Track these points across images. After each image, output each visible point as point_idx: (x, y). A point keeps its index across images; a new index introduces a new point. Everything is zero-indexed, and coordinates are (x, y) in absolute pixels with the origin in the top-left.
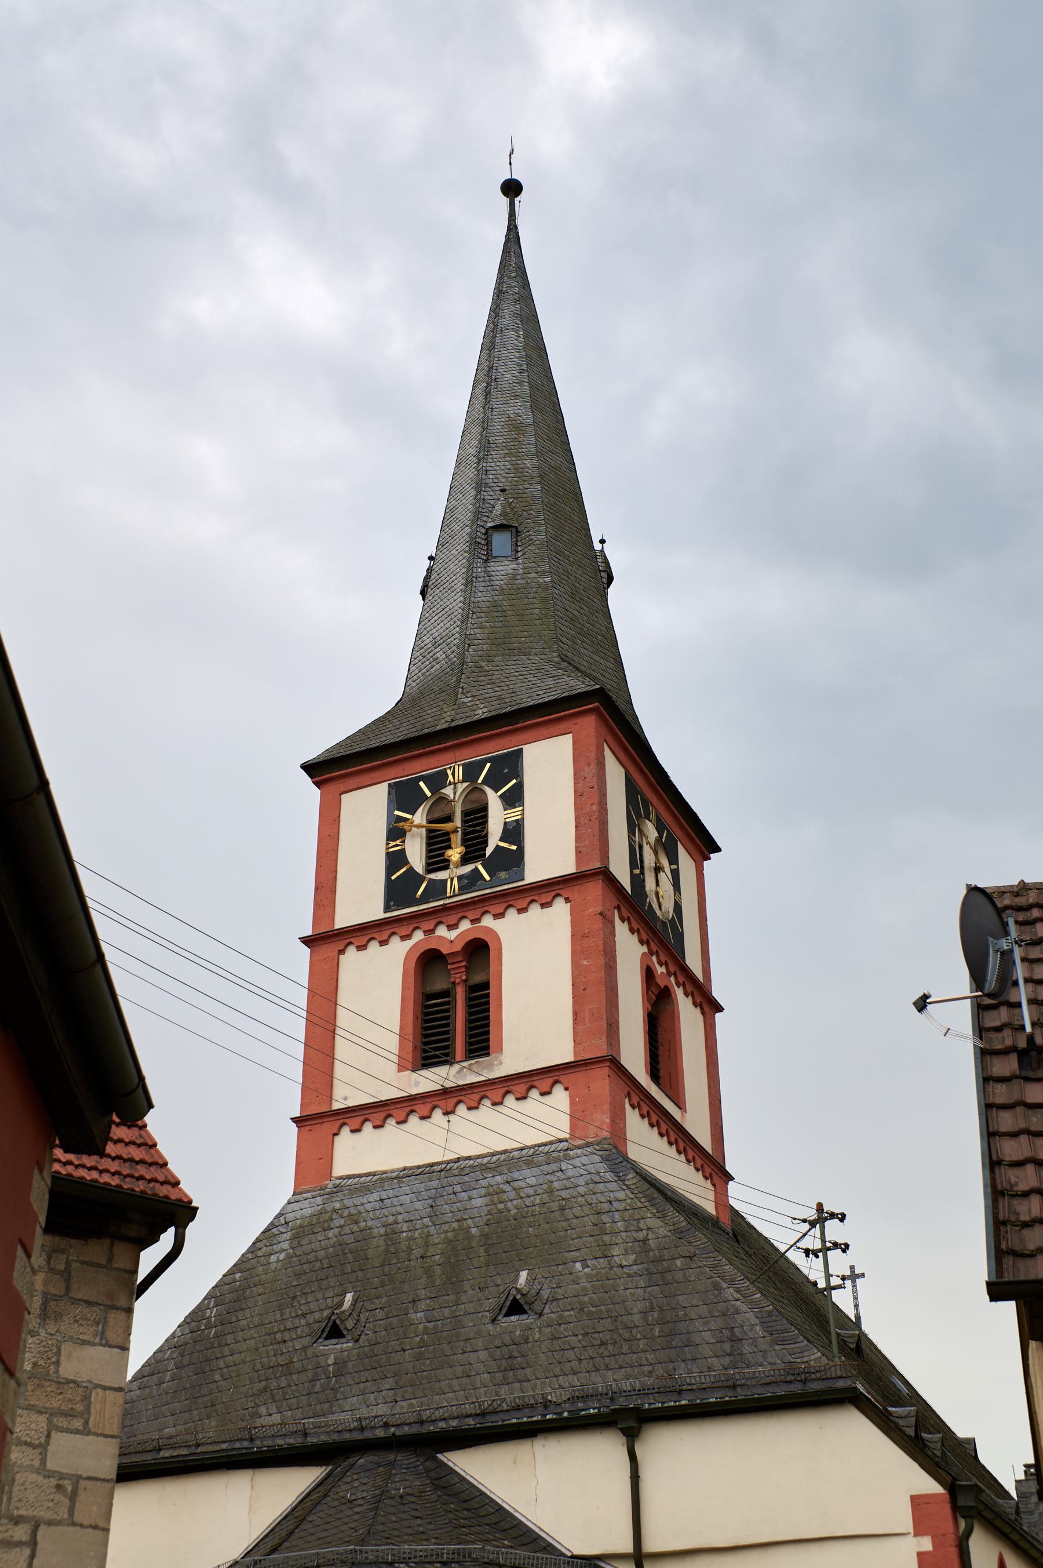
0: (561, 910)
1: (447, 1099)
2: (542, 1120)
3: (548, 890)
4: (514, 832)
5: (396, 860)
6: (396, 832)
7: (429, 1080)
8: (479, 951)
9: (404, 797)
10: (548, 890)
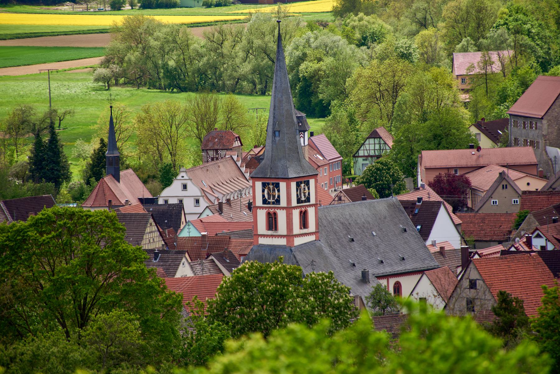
1: (272, 236)
2: (282, 242)
3: (283, 208)
4: (279, 196)
5: (263, 196)
6: (263, 191)
7: (270, 233)
8: (275, 214)
9: (264, 185)
10: (283, 208)
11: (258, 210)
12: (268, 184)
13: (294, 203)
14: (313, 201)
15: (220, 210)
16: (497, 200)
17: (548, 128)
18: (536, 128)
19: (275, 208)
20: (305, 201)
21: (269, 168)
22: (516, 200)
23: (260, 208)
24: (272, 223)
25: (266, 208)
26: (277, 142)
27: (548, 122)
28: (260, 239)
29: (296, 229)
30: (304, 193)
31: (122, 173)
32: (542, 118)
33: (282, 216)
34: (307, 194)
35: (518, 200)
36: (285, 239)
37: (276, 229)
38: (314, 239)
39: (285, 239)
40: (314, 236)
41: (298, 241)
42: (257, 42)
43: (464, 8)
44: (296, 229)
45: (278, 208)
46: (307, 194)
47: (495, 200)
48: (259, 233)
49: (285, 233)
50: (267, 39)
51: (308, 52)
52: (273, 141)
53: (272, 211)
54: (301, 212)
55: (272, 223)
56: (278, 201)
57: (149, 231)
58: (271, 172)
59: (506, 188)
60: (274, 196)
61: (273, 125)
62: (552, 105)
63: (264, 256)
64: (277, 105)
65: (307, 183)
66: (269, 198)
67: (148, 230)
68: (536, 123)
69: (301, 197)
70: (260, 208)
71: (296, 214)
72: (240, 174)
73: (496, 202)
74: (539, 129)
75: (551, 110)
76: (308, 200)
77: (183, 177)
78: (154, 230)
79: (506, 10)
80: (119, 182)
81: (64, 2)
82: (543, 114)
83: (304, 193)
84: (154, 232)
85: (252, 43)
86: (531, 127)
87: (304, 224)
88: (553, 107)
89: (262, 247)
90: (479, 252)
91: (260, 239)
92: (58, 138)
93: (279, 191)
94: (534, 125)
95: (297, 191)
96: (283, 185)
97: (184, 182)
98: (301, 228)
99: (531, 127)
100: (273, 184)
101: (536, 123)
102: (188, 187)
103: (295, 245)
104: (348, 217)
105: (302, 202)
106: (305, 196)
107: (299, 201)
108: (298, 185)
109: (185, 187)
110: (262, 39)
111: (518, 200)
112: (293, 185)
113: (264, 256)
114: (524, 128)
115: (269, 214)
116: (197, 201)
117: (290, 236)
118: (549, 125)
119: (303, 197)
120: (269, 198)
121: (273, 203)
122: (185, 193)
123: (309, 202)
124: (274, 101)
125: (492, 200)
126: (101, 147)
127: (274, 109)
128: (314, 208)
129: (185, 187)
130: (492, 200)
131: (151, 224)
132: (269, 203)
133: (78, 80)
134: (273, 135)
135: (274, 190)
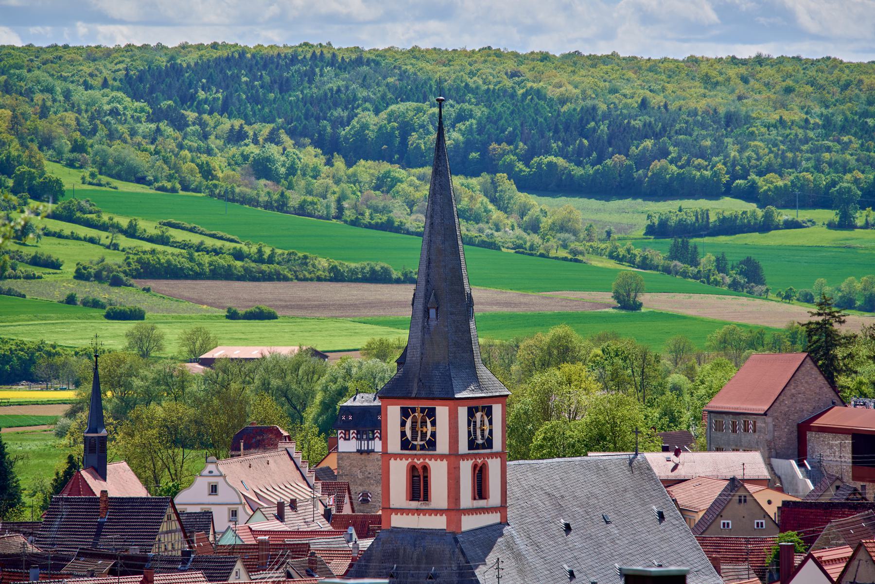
0: (445, 462)
1: (418, 511)
2: (439, 523)
3: (442, 457)
4: (433, 434)
5: (403, 434)
6: (403, 424)
7: (414, 505)
8: (425, 468)
9: (405, 413)
10: (442, 457)
11: (392, 462)
12: (414, 410)
13: (463, 447)
14: (497, 446)
15: (280, 517)
16: (730, 522)
17: (774, 430)
18: (754, 431)
19: (424, 456)
20: (483, 447)
21: (416, 380)
22: (760, 521)
23: (396, 456)
24: (419, 486)
25: (407, 457)
26: (432, 329)
27: (773, 421)
28: (393, 516)
29: (466, 499)
30: (483, 431)
31: (109, 467)
32: (765, 414)
33: (439, 472)
34: (487, 433)
35: (764, 521)
36: (444, 518)
37: (426, 498)
38: (498, 520)
39: (444, 518)
40: (499, 514)
41: (469, 523)
42: (275, 382)
43: (545, 348)
44: (466, 499)
45: (431, 457)
46: (487, 433)
47: (726, 521)
48: (392, 506)
49: (444, 505)
50: (288, 378)
51: (349, 384)
52: (424, 327)
53: (419, 462)
54: (475, 467)
55: (419, 486)
56: (432, 444)
57: (165, 529)
58: (419, 387)
59: (745, 501)
60: (424, 435)
61: (426, 295)
62: (780, 394)
63: (402, 551)
64: (433, 257)
65: (489, 412)
66: (414, 438)
67: (164, 527)
68: (755, 422)
69: (476, 438)
70: (396, 456)
71: (466, 468)
72: (301, 478)
73: (728, 524)
74: (760, 431)
75: (778, 402)
76: (489, 443)
77: (211, 472)
78: (174, 528)
79: (600, 352)
80: (105, 480)
81: (20, 381)
82: (766, 408)
83: (483, 431)
84: (175, 531)
85: (269, 384)
86: (746, 430)
87: (480, 491)
88: (781, 398)
89: (398, 532)
90: (816, 555)
91: (393, 516)
92: (6, 450)
93: (434, 423)
94: (750, 426)
95: (469, 425)
96: (442, 412)
97: (213, 480)
98: (475, 499)
99: (746, 430)
100: (422, 410)
101: (755, 422)
102: (220, 489)
103: (463, 529)
104: (559, 483)
105: (478, 447)
106: (483, 436)
107: (472, 445)
108: (471, 413)
109: (214, 489)
110: (283, 378)
111: (764, 521)
112: (463, 412)
113: (402, 551)
114: (734, 431)
115: (413, 469)
116: (234, 513)
117: (454, 510)
118: (775, 425)
119: (480, 437)
120: (414, 438)
121: (423, 448)
122: (213, 499)
123: (491, 448)
124: (429, 250)
125: (722, 522)
126: (70, 468)
127: (428, 267)
128: (499, 459)
129: (214, 489)
130: (722, 522)
131: (169, 518)
132: (414, 448)
133: (34, 440)
134: (424, 317)
135: (424, 423)
